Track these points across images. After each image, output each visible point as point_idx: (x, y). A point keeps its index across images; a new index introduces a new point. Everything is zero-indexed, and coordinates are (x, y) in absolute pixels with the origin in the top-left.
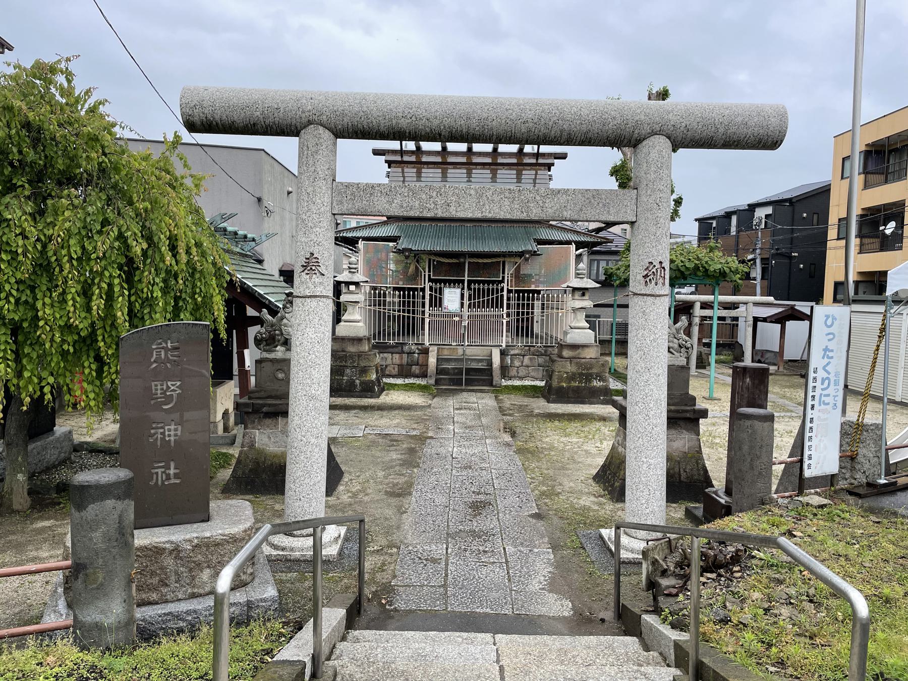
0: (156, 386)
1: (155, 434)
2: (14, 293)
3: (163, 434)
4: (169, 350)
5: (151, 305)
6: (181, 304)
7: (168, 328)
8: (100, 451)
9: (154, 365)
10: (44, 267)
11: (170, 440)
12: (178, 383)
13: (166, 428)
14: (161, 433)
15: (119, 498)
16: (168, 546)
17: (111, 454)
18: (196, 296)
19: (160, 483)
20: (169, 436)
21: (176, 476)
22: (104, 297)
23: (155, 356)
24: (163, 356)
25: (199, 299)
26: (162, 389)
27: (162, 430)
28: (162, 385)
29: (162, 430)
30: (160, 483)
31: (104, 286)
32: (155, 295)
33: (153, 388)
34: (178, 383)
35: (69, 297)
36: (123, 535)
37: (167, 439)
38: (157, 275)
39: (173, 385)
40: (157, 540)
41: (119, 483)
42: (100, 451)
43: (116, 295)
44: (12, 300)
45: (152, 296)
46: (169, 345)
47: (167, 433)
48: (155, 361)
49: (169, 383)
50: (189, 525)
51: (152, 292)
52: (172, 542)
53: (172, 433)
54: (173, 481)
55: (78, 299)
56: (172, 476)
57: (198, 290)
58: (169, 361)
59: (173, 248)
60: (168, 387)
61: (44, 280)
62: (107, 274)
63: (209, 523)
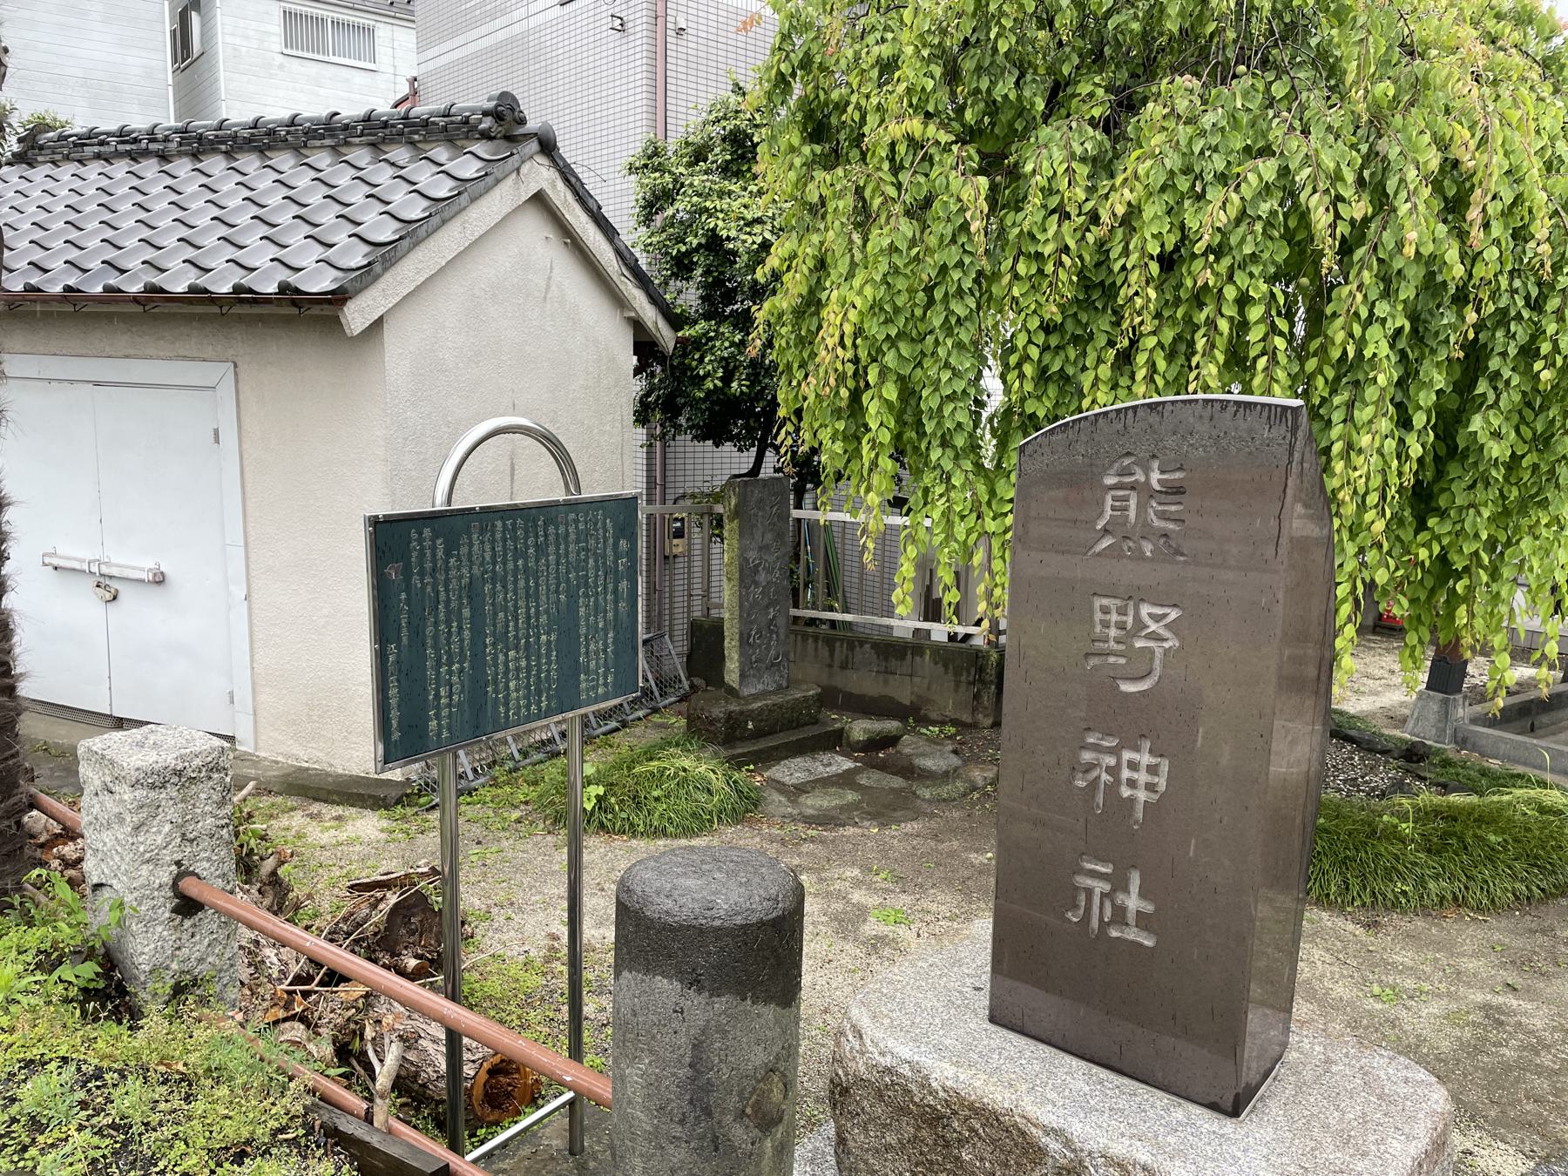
0: (1105, 610)
1: (1090, 767)
2: (1034, 352)
3: (1114, 771)
4: (1152, 494)
5: (1356, 384)
6: (1482, 387)
7: (1154, 418)
8: (1351, 740)
9: (1107, 542)
10: (1098, 289)
11: (1132, 800)
12: (1174, 614)
13: (1127, 755)
14: (1109, 770)
15: (695, 983)
16: (1054, 1146)
17: (1370, 750)
18: (1538, 366)
19: (1095, 923)
20: (1132, 783)
21: (1143, 921)
22: (1221, 358)
23: (1109, 512)
24: (1132, 514)
25: (1546, 375)
26: (1121, 626)
27: (1111, 761)
28: (1122, 612)
29: (1111, 761)
30: (1095, 923)
31: (1224, 325)
32: (1368, 353)
33: (1098, 616)
34: (1174, 614)
35: (1141, 358)
36: (708, 1112)
37: (1126, 792)
38: (1386, 294)
39: (1157, 618)
40: (1032, 1110)
41: (701, 931)
42: (1351, 740)
43: (1252, 354)
44: (1028, 369)
45: (1359, 353)
46: (1155, 476)
47: (1126, 774)
48: (1106, 531)
49: (1145, 610)
50: (1161, 1099)
51: (1361, 343)
52: (1068, 1143)
53: (1142, 777)
54: (1132, 934)
55: (1161, 365)
56: (1131, 917)
57: (1545, 348)
58: (1147, 532)
59: (1454, 207)
60: (1140, 625)
61: (1104, 323)
62: (1230, 293)
63: (1228, 1126)
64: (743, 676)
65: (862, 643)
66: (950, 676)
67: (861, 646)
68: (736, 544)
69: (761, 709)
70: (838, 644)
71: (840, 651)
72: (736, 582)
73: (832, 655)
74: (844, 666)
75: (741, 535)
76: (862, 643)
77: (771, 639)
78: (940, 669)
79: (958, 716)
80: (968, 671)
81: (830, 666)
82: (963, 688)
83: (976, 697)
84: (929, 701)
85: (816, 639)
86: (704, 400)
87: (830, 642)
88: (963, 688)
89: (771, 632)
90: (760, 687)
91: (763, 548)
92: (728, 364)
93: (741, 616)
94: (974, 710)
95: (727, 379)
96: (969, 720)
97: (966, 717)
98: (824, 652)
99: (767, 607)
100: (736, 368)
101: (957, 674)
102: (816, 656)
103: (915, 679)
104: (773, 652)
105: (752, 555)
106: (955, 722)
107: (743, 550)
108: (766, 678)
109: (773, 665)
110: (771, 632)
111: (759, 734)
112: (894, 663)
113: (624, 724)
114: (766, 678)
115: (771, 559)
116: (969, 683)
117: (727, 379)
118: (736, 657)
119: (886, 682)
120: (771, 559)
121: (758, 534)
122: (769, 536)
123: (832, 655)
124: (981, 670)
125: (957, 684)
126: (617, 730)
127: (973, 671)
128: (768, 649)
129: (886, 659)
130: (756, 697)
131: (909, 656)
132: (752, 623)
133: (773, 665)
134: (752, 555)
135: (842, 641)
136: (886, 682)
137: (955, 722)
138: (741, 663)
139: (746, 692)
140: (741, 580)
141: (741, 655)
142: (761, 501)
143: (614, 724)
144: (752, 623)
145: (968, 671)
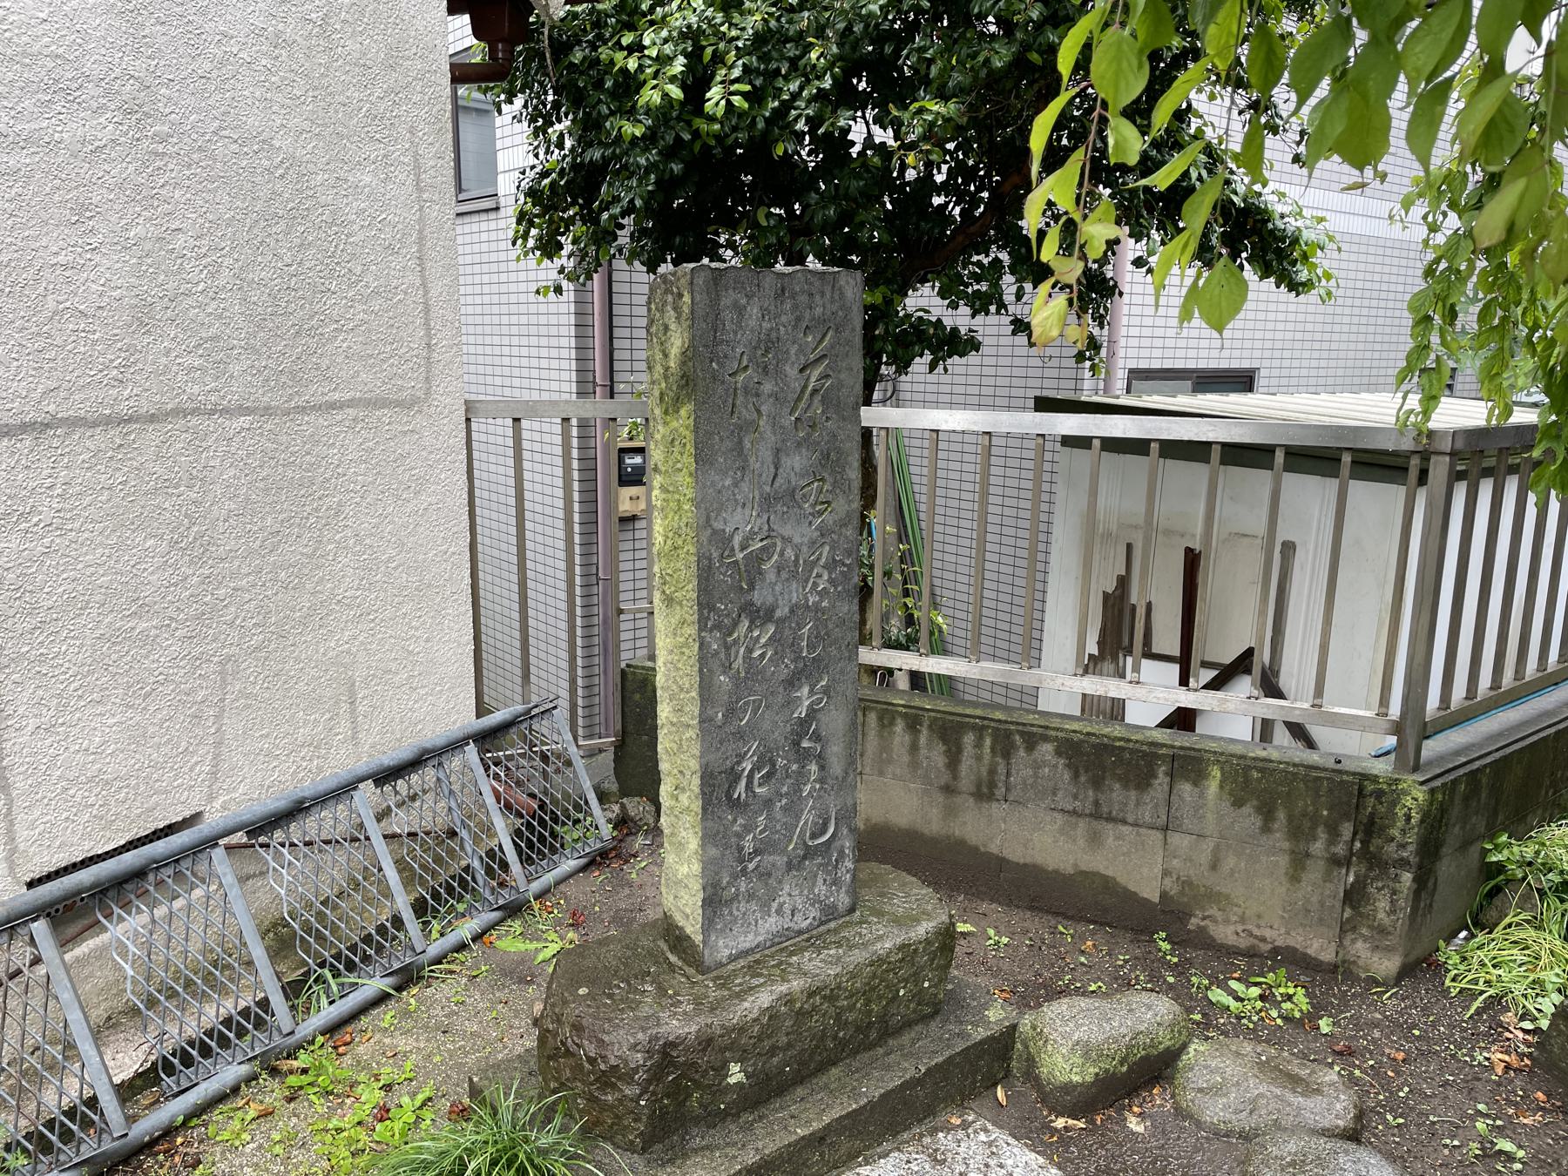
64: (714, 902)
65: (1032, 740)
66: (1279, 838)
67: (1030, 747)
68: (685, 480)
69: (772, 1013)
70: (969, 739)
71: (975, 757)
72: (689, 612)
73: (953, 761)
74: (985, 792)
75: (703, 458)
76: (1032, 740)
77: (802, 775)
78: (1248, 818)
79: (1296, 940)
80: (1334, 834)
81: (949, 790)
82: (1314, 873)
83: (1354, 897)
84: (1213, 897)
85: (913, 724)
86: (650, 138)
87: (949, 732)
88: (1314, 873)
89: (803, 756)
90: (772, 924)
91: (778, 499)
92: (699, 50)
93: (705, 720)
94: (1347, 928)
95: (696, 84)
96: (1328, 956)
97: (1321, 948)
98: (934, 755)
99: (791, 683)
100: (718, 59)
101: (1299, 833)
102: (914, 765)
103: (1175, 839)
104: (808, 817)
105: (741, 522)
106: (1297, 963)
107: (708, 508)
108: (790, 894)
109: (809, 853)
110: (803, 756)
111: (766, 1091)
112: (1116, 794)
113: (408, 977)
114: (790, 894)
115: (801, 533)
116: (1335, 862)
117: (696, 84)
118: (693, 844)
119: (1095, 839)
120: (801, 533)
121: (760, 456)
122: (796, 462)
123: (953, 761)
124: (1370, 829)
125: (1299, 861)
126: (382, 999)
127: (1347, 830)
128: (793, 810)
129: (1097, 783)
130: (756, 963)
131: (1162, 779)
132: (740, 735)
133: (809, 853)
134: (741, 522)
135: (980, 731)
136: (1095, 839)
137: (1297, 963)
138: (707, 864)
139: (724, 948)
140: (705, 604)
141: (708, 838)
142: (770, 343)
143: (375, 984)
144: (740, 735)
145: (1334, 834)
